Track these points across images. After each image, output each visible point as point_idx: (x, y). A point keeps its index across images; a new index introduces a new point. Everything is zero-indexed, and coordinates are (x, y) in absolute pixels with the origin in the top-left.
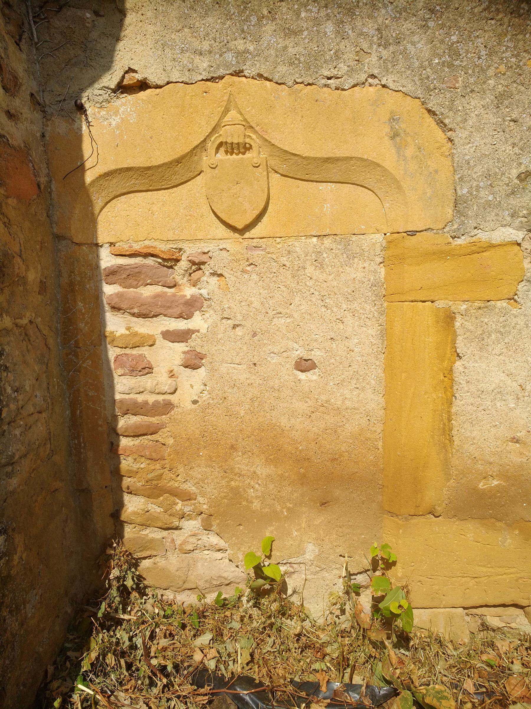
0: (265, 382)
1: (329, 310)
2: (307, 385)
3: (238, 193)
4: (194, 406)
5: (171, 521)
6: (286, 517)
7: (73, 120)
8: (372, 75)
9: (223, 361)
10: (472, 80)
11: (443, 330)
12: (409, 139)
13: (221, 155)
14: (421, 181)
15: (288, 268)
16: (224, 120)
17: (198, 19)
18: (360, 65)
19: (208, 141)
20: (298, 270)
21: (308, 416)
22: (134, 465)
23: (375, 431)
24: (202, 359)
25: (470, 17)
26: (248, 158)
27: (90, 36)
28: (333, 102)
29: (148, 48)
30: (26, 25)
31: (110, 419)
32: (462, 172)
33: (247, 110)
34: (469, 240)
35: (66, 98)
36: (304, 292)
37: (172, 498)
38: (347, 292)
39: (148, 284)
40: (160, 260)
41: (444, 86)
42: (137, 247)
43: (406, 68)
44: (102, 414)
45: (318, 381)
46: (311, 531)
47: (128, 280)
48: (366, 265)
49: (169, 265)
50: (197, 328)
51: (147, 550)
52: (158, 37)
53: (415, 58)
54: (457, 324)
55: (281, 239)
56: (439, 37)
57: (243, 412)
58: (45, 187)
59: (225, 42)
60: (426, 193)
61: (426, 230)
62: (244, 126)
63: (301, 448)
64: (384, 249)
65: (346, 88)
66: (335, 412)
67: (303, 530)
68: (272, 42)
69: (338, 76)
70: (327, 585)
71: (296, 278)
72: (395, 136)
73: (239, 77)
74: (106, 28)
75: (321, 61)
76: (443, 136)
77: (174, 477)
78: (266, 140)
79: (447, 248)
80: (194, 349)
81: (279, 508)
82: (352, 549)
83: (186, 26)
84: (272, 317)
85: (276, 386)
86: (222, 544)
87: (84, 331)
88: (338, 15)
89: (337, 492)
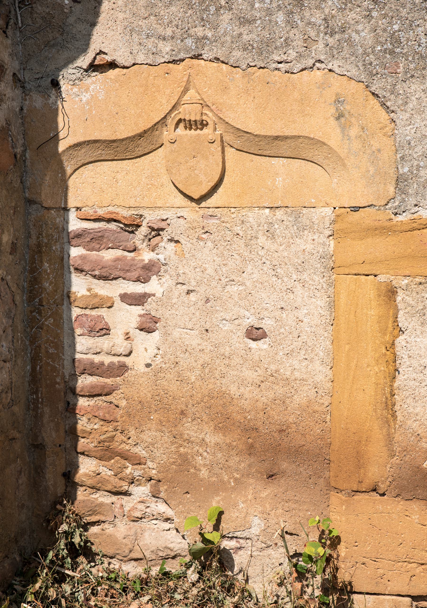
0: (216, 349)
1: (280, 280)
2: (257, 353)
3: (195, 166)
4: (147, 370)
5: (120, 485)
6: (233, 487)
7: (49, 96)
8: (319, 60)
9: (176, 326)
10: (412, 66)
11: (385, 304)
12: (353, 120)
13: (181, 129)
14: (365, 159)
15: (241, 238)
16: (183, 99)
17: (163, 8)
18: (307, 51)
19: (168, 117)
20: (251, 240)
21: (257, 386)
22: (87, 425)
23: (323, 404)
24: (156, 323)
25: (411, 7)
26: (204, 135)
27: (67, 20)
28: (283, 84)
29: (118, 33)
30: (13, 12)
31: (67, 378)
32: (403, 151)
33: (204, 90)
34: (410, 216)
35: (44, 76)
36: (256, 261)
37: (123, 461)
38: (297, 262)
39: (109, 248)
40: (122, 226)
41: (386, 71)
42: (101, 212)
43: (351, 55)
44: (61, 372)
45: (268, 350)
46: (258, 504)
47: (91, 243)
48: (315, 237)
49: (130, 230)
50: (153, 292)
51: (95, 515)
52: (127, 23)
53: (359, 45)
54: (399, 299)
55: (235, 209)
56: (382, 26)
57: (194, 378)
58: (21, 156)
59: (187, 28)
60: (369, 171)
61: (369, 206)
62: (202, 104)
63: (249, 417)
64: (334, 222)
65: (295, 71)
66: (284, 382)
67: (249, 502)
68: (228, 29)
69: (287, 61)
70: (273, 564)
71: (249, 247)
72: (339, 116)
73: (198, 59)
74: (81, 14)
75: (273, 47)
76: (387, 117)
77: (125, 439)
78: (221, 119)
79: (388, 224)
80: (149, 313)
81: (226, 478)
82: (297, 525)
83: (152, 14)
84: (225, 284)
85: (227, 354)
86: (170, 513)
87: (48, 291)
88: (288, 6)
89: (284, 465)
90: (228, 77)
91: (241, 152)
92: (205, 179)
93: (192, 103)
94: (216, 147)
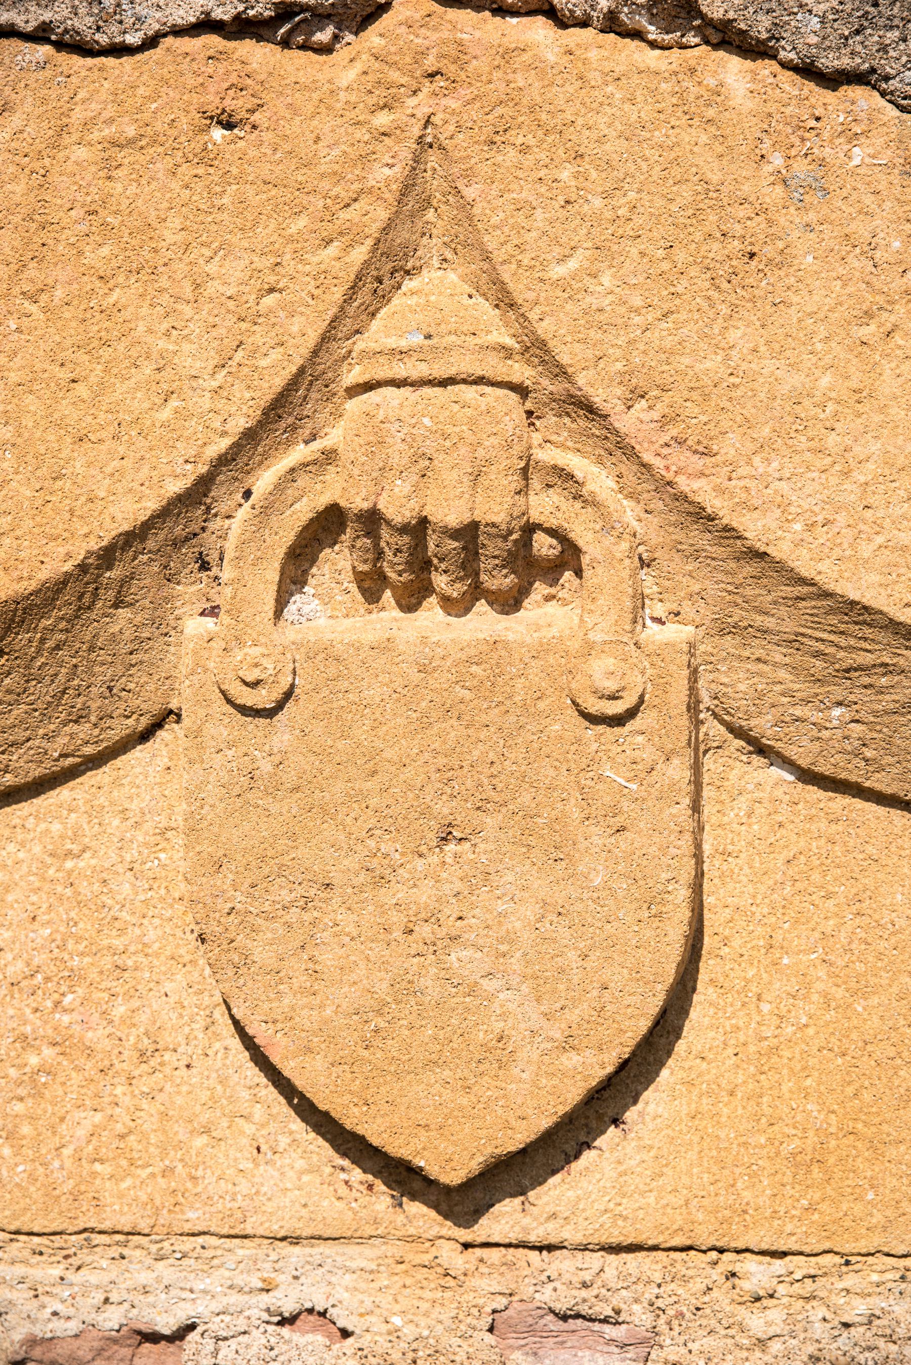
3: (451, 910)
13: (326, 600)
16: (361, 344)
26: (541, 651)
33: (558, 271)
55: (779, 1266)
62: (522, 391)
90: (778, 160)
91: (841, 802)
92: (536, 1021)
93: (444, 383)
94: (648, 755)
